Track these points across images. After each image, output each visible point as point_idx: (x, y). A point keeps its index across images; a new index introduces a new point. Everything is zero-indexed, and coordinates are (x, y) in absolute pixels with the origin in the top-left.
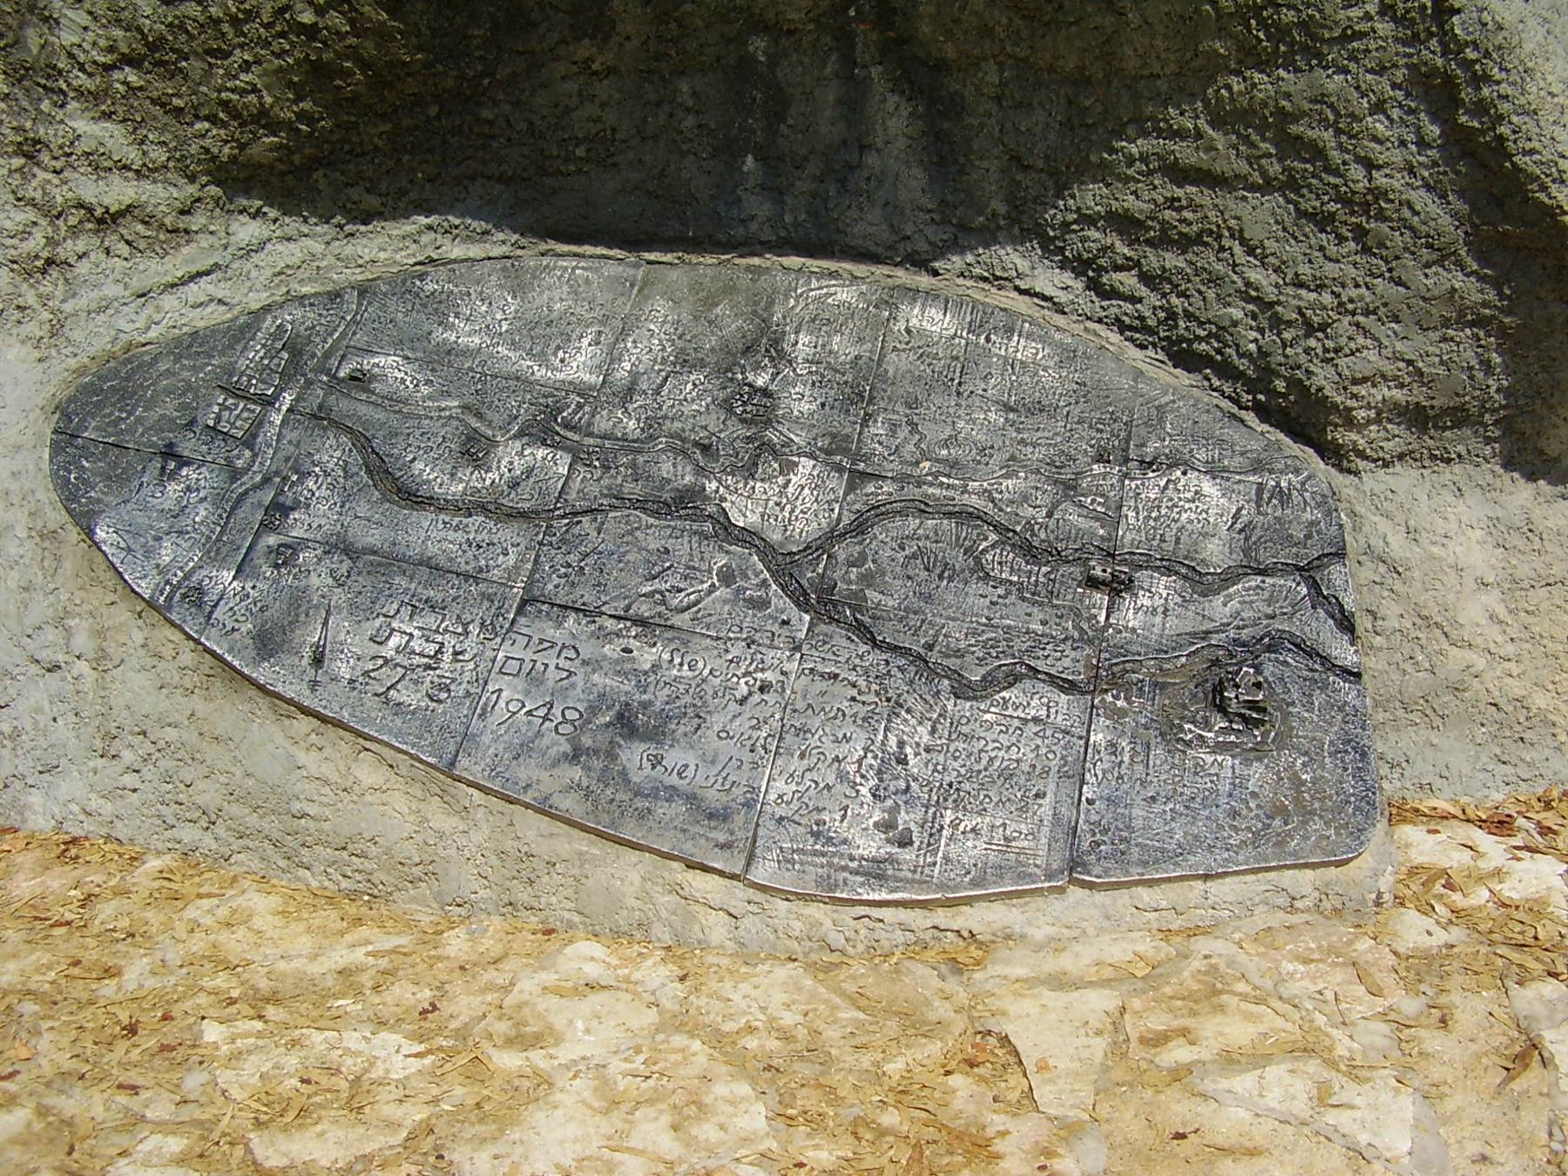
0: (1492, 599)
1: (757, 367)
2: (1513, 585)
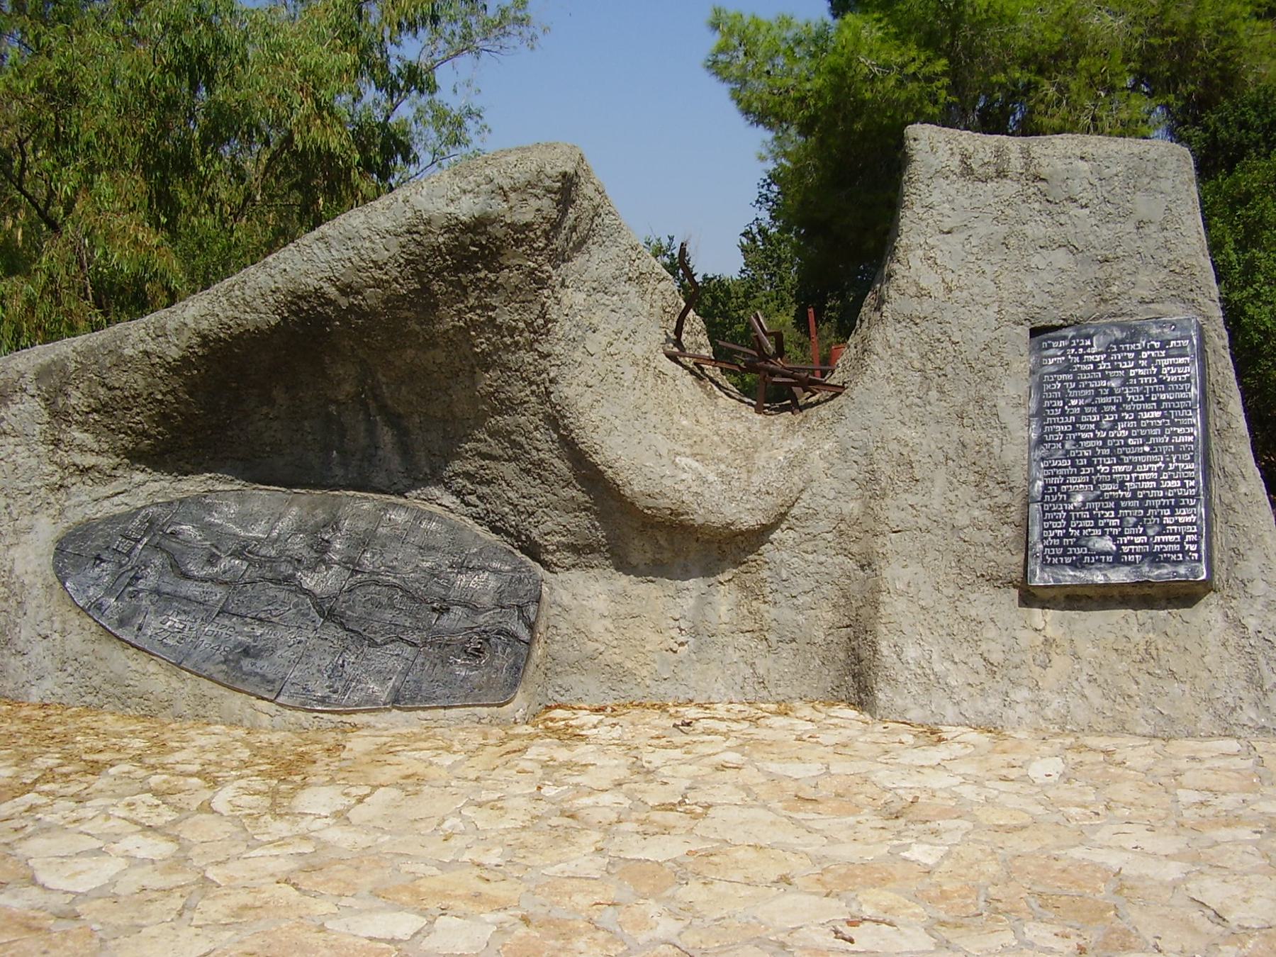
0: (607, 623)
1: (327, 532)
2: (616, 617)
